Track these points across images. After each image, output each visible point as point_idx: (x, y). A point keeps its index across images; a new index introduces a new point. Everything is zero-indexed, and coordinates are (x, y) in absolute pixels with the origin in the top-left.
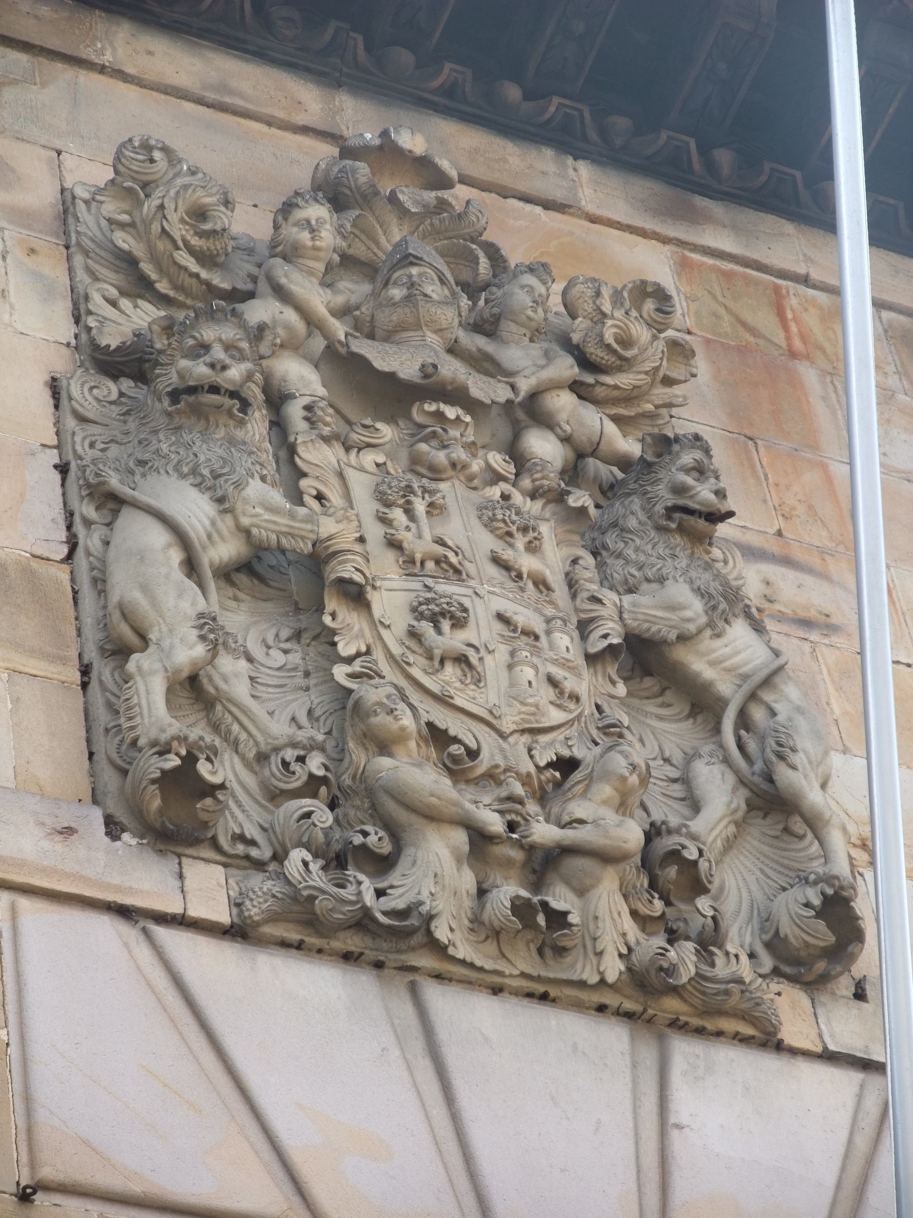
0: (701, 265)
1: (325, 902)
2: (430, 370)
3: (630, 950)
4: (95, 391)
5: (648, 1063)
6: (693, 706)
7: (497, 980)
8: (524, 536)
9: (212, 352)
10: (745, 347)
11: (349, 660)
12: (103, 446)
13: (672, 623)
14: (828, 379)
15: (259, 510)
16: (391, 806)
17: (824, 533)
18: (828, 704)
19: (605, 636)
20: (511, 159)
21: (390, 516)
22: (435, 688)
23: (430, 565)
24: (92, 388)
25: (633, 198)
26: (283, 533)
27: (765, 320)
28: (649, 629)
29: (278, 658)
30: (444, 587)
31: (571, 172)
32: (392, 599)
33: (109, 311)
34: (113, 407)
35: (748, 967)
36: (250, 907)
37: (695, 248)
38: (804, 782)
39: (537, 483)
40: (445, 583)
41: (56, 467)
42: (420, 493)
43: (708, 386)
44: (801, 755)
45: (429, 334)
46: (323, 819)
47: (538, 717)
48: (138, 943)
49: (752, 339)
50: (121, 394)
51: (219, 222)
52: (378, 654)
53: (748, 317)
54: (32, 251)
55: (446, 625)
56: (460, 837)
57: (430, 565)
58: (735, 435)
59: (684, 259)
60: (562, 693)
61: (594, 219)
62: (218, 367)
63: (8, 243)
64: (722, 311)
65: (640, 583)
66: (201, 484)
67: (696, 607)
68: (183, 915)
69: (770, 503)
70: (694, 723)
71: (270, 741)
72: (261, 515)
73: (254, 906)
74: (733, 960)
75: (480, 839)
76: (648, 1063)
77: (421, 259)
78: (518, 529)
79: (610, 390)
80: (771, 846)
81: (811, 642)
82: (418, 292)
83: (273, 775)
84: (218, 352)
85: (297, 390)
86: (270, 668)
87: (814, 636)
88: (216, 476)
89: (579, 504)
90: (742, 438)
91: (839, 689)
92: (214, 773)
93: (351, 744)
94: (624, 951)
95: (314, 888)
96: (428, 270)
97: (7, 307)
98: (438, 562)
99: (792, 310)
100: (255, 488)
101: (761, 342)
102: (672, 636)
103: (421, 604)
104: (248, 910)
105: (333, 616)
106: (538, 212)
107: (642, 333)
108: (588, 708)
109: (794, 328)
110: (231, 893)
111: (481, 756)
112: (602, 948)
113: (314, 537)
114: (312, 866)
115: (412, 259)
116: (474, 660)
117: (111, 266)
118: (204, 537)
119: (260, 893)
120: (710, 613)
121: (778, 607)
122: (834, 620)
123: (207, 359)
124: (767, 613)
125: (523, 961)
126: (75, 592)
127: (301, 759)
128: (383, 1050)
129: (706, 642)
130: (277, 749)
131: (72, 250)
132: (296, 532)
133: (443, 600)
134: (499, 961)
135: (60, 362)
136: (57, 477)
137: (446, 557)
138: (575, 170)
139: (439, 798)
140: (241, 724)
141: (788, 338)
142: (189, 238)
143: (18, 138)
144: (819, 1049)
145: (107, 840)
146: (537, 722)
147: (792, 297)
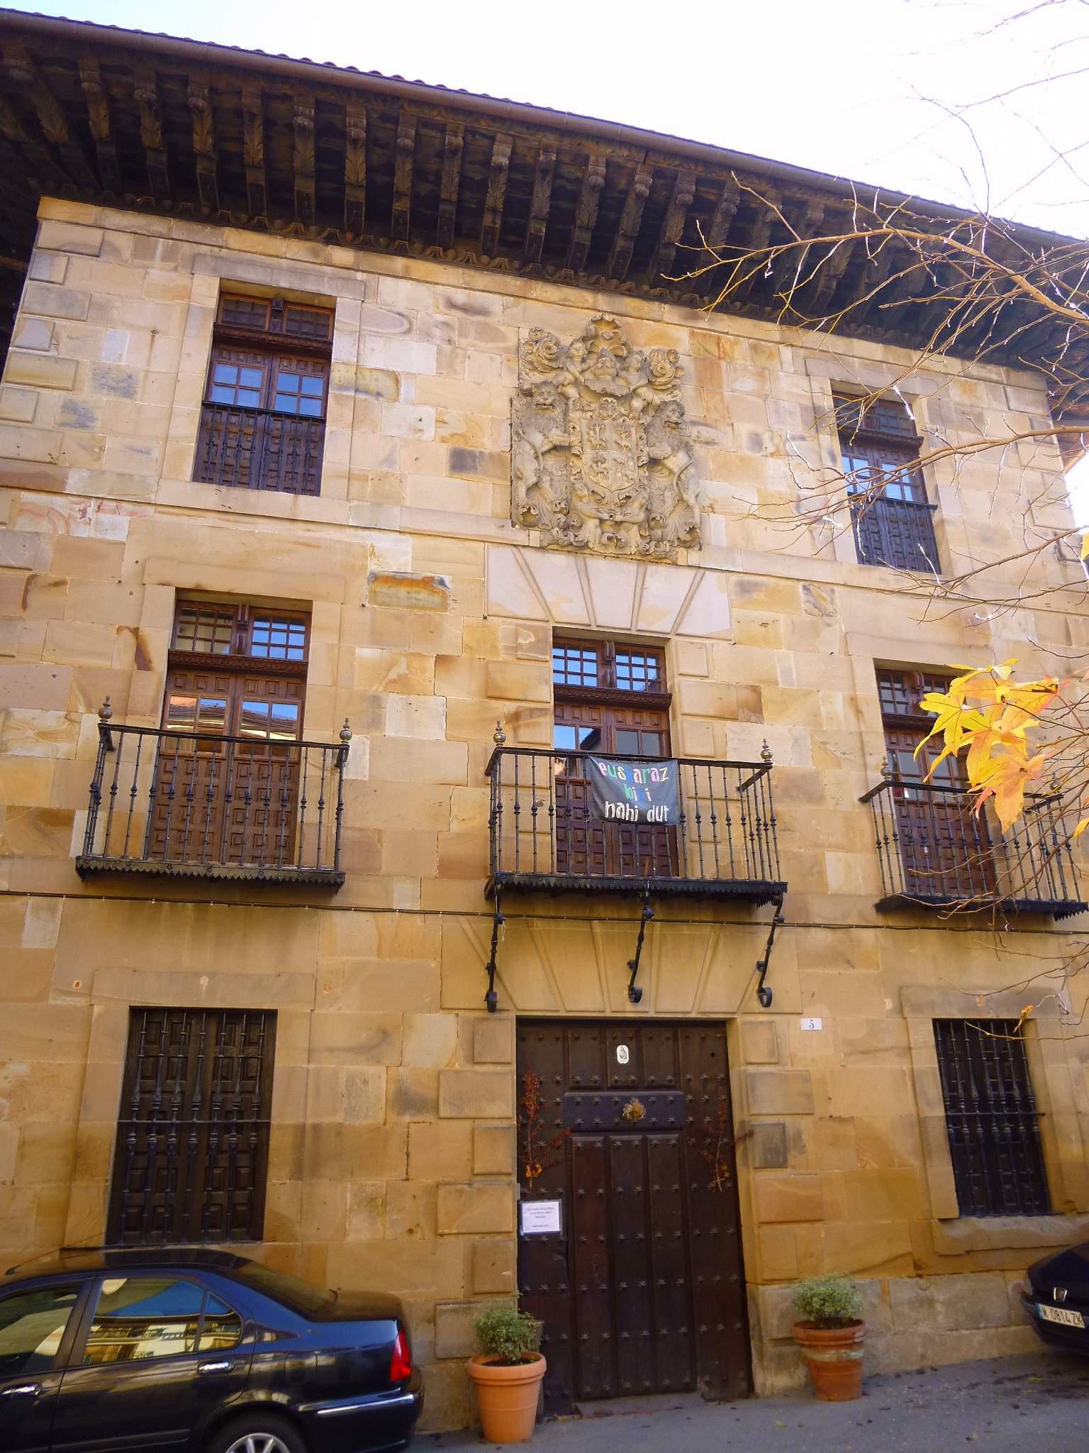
30: (602, 452)
32: (588, 455)
75: (602, 521)
100: (554, 431)
107: (668, 366)
135: (513, 393)
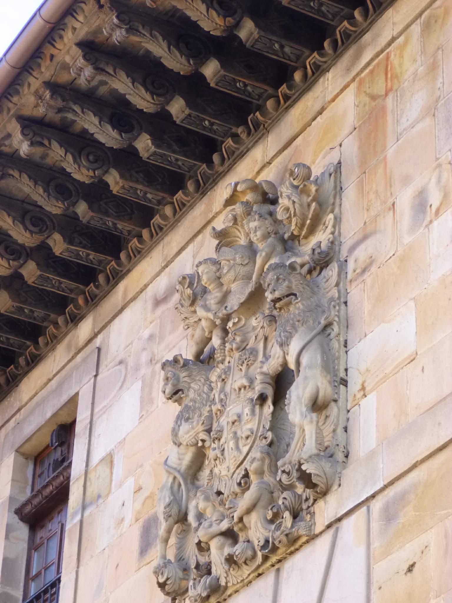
47: (238, 459)
118: (178, 461)
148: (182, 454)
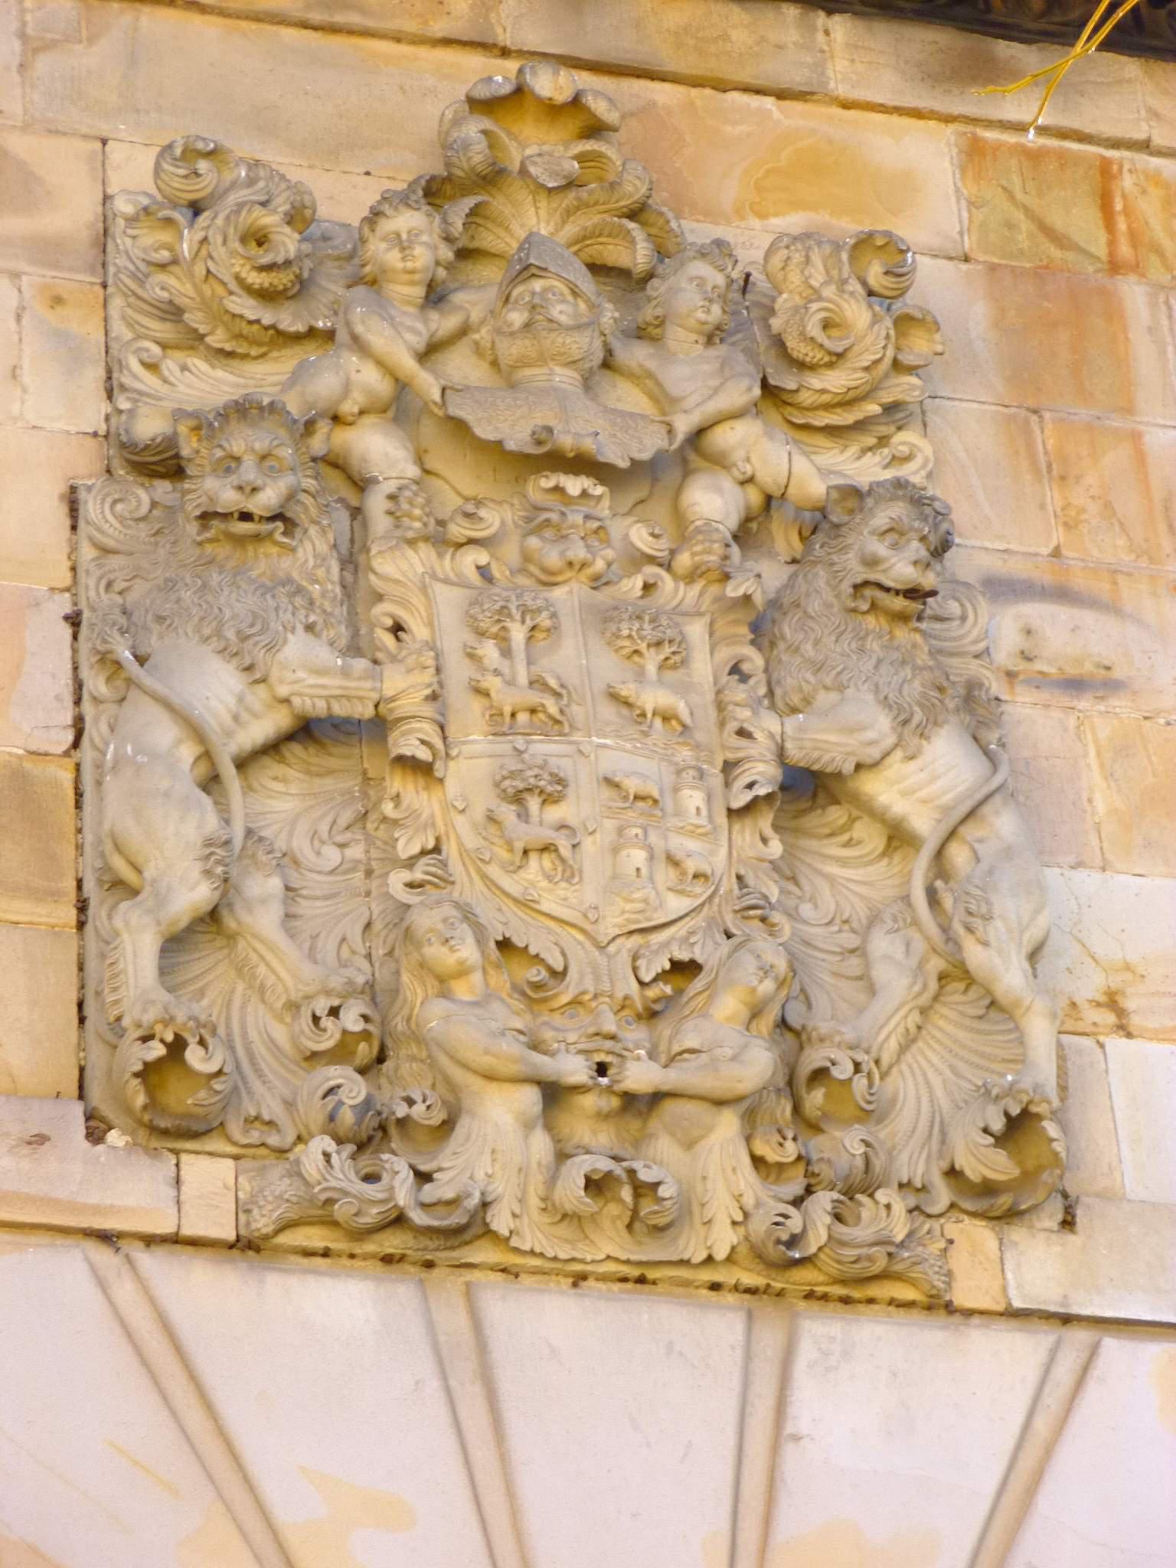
0: (997, 147)
1: (346, 1207)
2: (543, 436)
3: (746, 1215)
4: (119, 507)
5: (769, 1353)
6: (890, 838)
7: (578, 1267)
8: (657, 654)
9: (243, 469)
10: (1047, 267)
11: (410, 863)
12: (125, 585)
13: (849, 749)
14: (1162, 298)
15: (301, 674)
16: (444, 1061)
17: (1121, 542)
18: (1090, 801)
19: (750, 786)
20: (735, 35)
21: (480, 652)
22: (514, 889)
23: (523, 717)
24: (115, 502)
25: (906, 62)
26: (336, 697)
27: (1081, 221)
28: (818, 759)
29: (332, 856)
31: (820, 37)
32: (473, 767)
33: (150, 381)
34: (142, 525)
35: (902, 1219)
36: (258, 1217)
37: (990, 124)
38: (997, 961)
39: (697, 558)
40: (540, 741)
41: (67, 618)
42: (518, 617)
43: (984, 340)
44: (998, 923)
45: (558, 370)
46: (353, 1094)
47: (648, 914)
48: (119, 1275)
49: (1056, 253)
50: (154, 504)
51: (282, 249)
52: (450, 849)
53: (1057, 220)
54: (57, 301)
55: (533, 803)
56: (530, 1098)
57: (523, 717)
58: (1013, 410)
59: (976, 140)
60: (684, 873)
61: (847, 105)
62: (248, 489)
63: (27, 294)
64: (1019, 216)
65: (815, 690)
66: (225, 649)
67: (882, 725)
68: (177, 1234)
69: (1050, 508)
70: (889, 864)
71: (300, 987)
72: (303, 680)
73: (264, 1216)
74: (883, 1213)
76: (769, 1353)
77: (545, 270)
78: (649, 646)
79: (817, 395)
80: (972, 1030)
81: (1080, 711)
82: (540, 317)
83: (302, 1032)
84: (249, 472)
85: (381, 473)
86: (319, 872)
87: (1084, 703)
88: (244, 638)
89: (740, 592)
90: (1023, 413)
91: (1109, 776)
92: (208, 1059)
93: (405, 978)
94: (739, 1217)
95: (334, 1189)
96: (557, 283)
97: (19, 391)
98: (533, 711)
99: (1124, 197)
100: (297, 648)
101: (1070, 256)
102: (848, 767)
103: (504, 778)
104: (255, 1221)
105: (397, 798)
106: (769, 106)
108: (729, 884)
109: (1122, 225)
110: (241, 1195)
111: (568, 978)
112: (710, 1216)
113: (375, 696)
114: (335, 1159)
115: (534, 271)
116: (565, 851)
117: (155, 311)
118: (228, 720)
119: (270, 1198)
120: (899, 729)
121: (1038, 666)
122: (1117, 674)
123: (234, 479)
124: (1021, 677)
125: (609, 1244)
126: (79, 795)
127: (334, 1012)
128: (417, 1383)
129: (896, 765)
130: (308, 998)
131: (110, 290)
132: (353, 693)
133: (530, 773)
134: (580, 1245)
136: (67, 631)
137: (543, 705)
138: (827, 33)
139: (495, 1056)
140: (268, 965)
141: (1112, 243)
142: (243, 275)
143: (50, 131)
144: (1000, 1308)
145: (86, 1144)
146: (648, 920)
147: (1126, 176)
148: (248, 710)
